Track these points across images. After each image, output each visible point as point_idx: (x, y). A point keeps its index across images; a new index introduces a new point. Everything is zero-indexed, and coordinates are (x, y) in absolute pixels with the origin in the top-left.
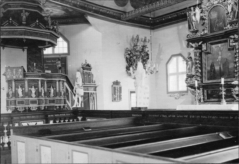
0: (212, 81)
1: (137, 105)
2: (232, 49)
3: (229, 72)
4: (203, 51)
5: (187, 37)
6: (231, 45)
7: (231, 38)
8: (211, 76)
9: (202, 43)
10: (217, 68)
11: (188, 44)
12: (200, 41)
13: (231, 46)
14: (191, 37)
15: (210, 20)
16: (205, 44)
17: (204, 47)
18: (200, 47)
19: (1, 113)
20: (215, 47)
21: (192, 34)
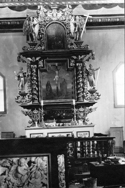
0: (49, 101)
1: (30, 136)
2: (71, 69)
3: (67, 93)
4: (40, 68)
5: (24, 50)
6: (71, 65)
7: (73, 59)
8: (47, 95)
9: (40, 60)
10: (54, 88)
11: (19, 57)
12: (38, 57)
13: (72, 67)
14: (28, 49)
15: (48, 36)
16: (42, 60)
17: (41, 64)
18: (37, 63)
19: (124, 29)
20: (52, 66)
21: (29, 46)
